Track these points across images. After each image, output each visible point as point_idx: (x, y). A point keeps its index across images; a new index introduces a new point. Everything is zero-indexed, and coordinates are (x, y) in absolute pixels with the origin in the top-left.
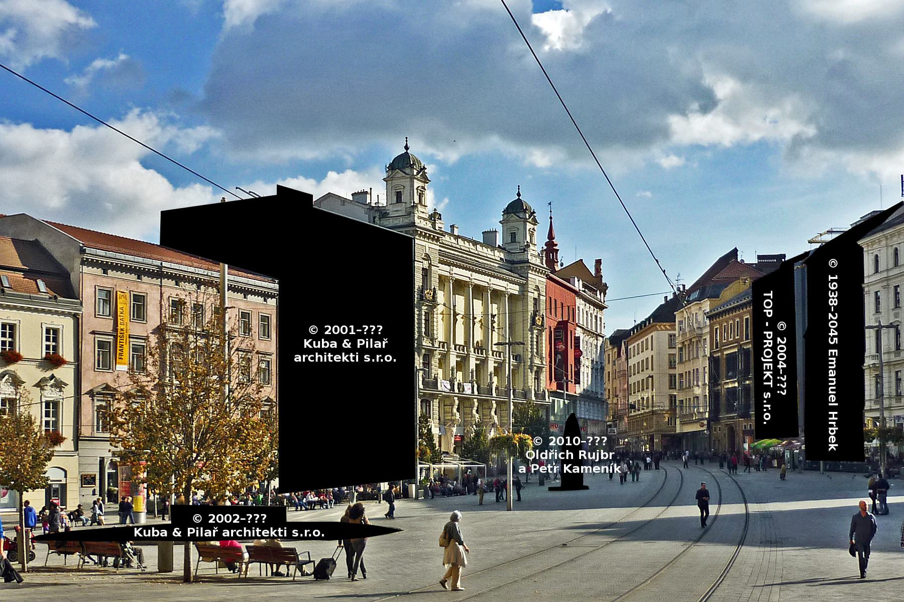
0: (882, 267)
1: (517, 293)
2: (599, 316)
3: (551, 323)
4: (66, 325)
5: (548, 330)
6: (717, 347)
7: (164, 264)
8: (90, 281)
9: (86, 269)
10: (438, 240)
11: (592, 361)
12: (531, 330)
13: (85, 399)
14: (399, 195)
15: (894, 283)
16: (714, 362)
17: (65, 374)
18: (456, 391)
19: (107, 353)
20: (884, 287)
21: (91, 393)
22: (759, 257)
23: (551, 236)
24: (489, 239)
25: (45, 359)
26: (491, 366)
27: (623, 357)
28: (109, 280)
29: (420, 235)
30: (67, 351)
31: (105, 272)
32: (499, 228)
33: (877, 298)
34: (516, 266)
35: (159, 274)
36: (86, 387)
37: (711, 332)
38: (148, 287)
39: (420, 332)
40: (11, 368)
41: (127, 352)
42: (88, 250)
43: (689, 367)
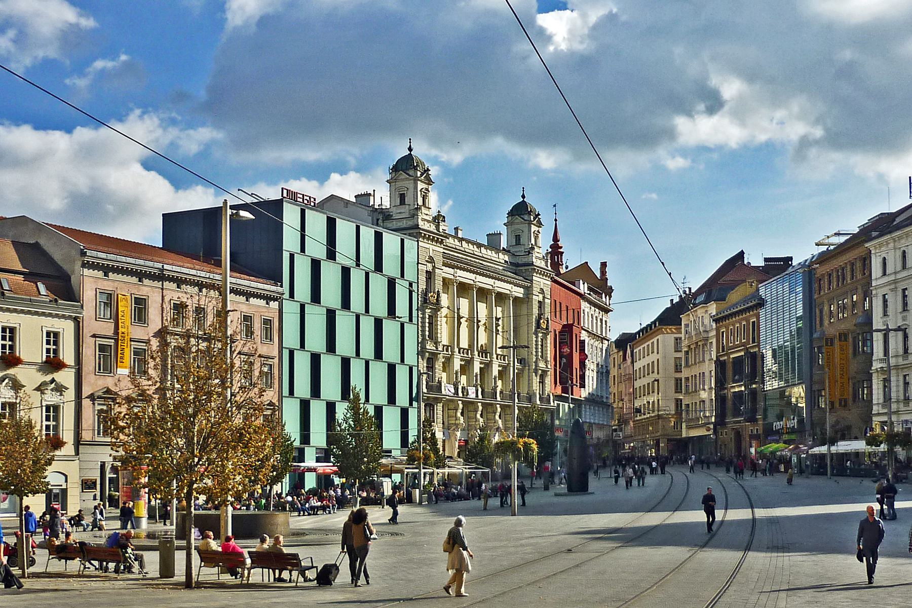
0: (889, 270)
1: (521, 296)
2: (604, 319)
3: (556, 326)
4: (66, 329)
6: (723, 351)
7: (166, 267)
8: (90, 284)
9: (86, 272)
10: (441, 242)
11: (598, 365)
12: (536, 334)
13: (86, 403)
14: (402, 197)
15: (901, 286)
16: (720, 365)
17: (66, 377)
18: (460, 394)
19: (108, 357)
20: (892, 290)
21: (92, 397)
22: (766, 260)
23: (556, 239)
24: (493, 241)
25: (46, 362)
26: (495, 370)
27: (629, 360)
28: (110, 283)
30: (67, 355)
31: (106, 275)
32: (504, 230)
33: (885, 301)
34: (521, 268)
35: (161, 277)
36: (86, 391)
37: (717, 335)
38: (149, 290)
40: (11, 371)
41: (128, 356)
42: (89, 253)
43: (695, 371)
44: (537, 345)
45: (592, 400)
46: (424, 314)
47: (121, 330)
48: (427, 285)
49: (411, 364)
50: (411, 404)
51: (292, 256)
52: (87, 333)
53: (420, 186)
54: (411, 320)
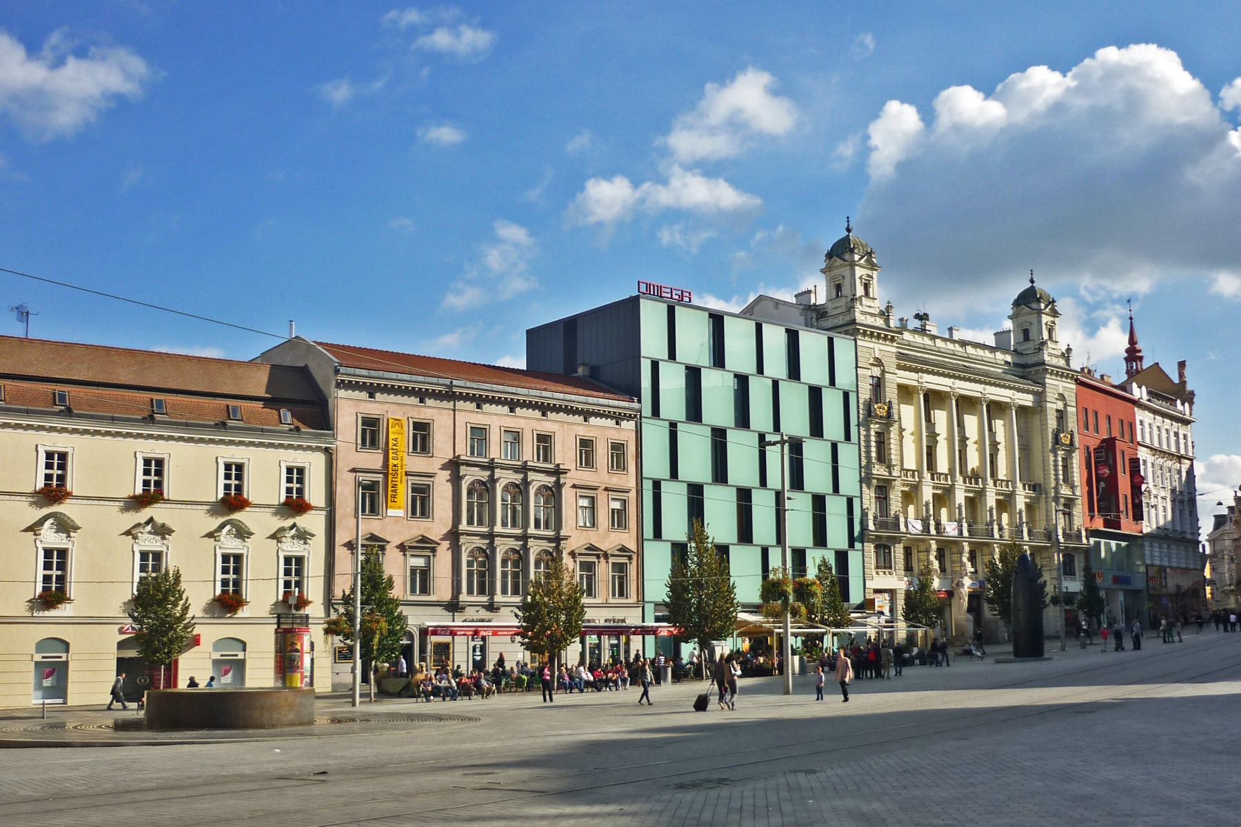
1: (1030, 404)
2: (1181, 432)
3: (1085, 441)
4: (314, 464)
5: (1083, 451)
7: (455, 382)
8: (348, 409)
9: (342, 393)
10: (893, 340)
11: (1173, 491)
12: (1054, 451)
13: (341, 553)
17: (314, 522)
18: (933, 531)
19: (372, 497)
21: (350, 546)
25: (285, 504)
26: (991, 500)
29: (1052, 374)
30: (315, 493)
31: (372, 396)
32: (1008, 325)
34: (1029, 369)
35: (450, 395)
36: (342, 537)
38: (436, 413)
39: (1057, 479)
40: (237, 516)
41: (404, 493)
42: (342, 370)
44: (1056, 466)
45: (1161, 536)
46: (868, 430)
47: (391, 462)
48: (1058, 425)
49: (850, 494)
50: (851, 545)
51: (655, 365)
52: (343, 466)
53: (859, 272)
54: (848, 437)
